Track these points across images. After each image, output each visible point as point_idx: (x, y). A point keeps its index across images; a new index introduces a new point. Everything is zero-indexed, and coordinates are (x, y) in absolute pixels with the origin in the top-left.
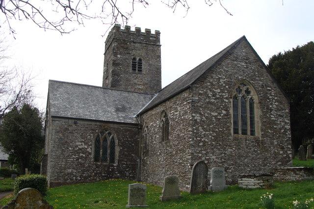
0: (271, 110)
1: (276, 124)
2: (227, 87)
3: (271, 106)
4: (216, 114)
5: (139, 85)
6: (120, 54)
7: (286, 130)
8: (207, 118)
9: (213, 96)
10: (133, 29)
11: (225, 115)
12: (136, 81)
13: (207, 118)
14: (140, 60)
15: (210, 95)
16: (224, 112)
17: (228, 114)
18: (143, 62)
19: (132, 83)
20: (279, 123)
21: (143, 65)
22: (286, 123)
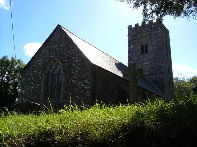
0: (74, 76)
1: (76, 87)
2: (42, 67)
3: (73, 73)
4: (33, 87)
5: (146, 62)
6: (132, 44)
7: (85, 91)
8: (28, 91)
9: (33, 75)
10: (134, 26)
11: (38, 87)
12: (143, 60)
13: (28, 91)
14: (146, 44)
15: (31, 76)
16: (38, 85)
17: (40, 87)
18: (149, 45)
19: (141, 61)
20: (79, 85)
21: (148, 47)
22: (86, 84)
